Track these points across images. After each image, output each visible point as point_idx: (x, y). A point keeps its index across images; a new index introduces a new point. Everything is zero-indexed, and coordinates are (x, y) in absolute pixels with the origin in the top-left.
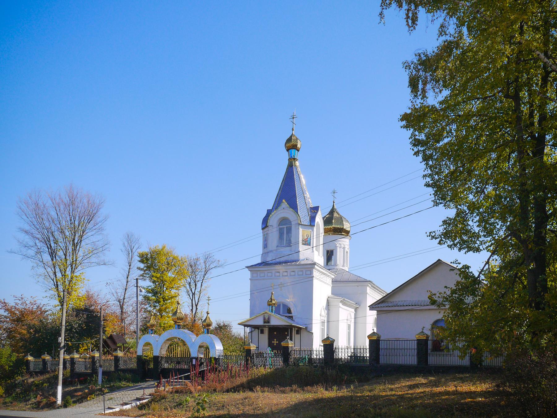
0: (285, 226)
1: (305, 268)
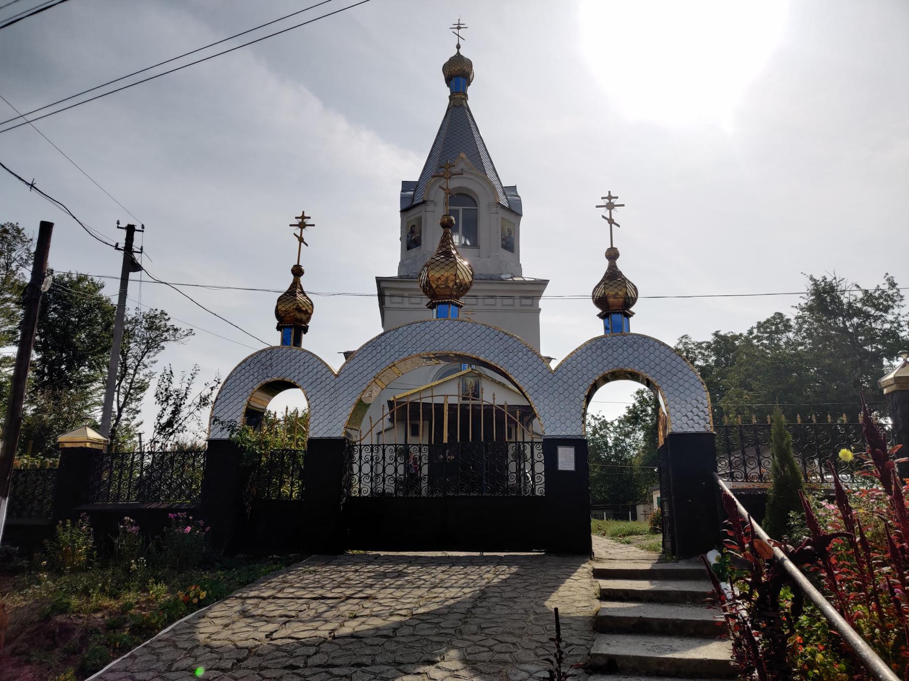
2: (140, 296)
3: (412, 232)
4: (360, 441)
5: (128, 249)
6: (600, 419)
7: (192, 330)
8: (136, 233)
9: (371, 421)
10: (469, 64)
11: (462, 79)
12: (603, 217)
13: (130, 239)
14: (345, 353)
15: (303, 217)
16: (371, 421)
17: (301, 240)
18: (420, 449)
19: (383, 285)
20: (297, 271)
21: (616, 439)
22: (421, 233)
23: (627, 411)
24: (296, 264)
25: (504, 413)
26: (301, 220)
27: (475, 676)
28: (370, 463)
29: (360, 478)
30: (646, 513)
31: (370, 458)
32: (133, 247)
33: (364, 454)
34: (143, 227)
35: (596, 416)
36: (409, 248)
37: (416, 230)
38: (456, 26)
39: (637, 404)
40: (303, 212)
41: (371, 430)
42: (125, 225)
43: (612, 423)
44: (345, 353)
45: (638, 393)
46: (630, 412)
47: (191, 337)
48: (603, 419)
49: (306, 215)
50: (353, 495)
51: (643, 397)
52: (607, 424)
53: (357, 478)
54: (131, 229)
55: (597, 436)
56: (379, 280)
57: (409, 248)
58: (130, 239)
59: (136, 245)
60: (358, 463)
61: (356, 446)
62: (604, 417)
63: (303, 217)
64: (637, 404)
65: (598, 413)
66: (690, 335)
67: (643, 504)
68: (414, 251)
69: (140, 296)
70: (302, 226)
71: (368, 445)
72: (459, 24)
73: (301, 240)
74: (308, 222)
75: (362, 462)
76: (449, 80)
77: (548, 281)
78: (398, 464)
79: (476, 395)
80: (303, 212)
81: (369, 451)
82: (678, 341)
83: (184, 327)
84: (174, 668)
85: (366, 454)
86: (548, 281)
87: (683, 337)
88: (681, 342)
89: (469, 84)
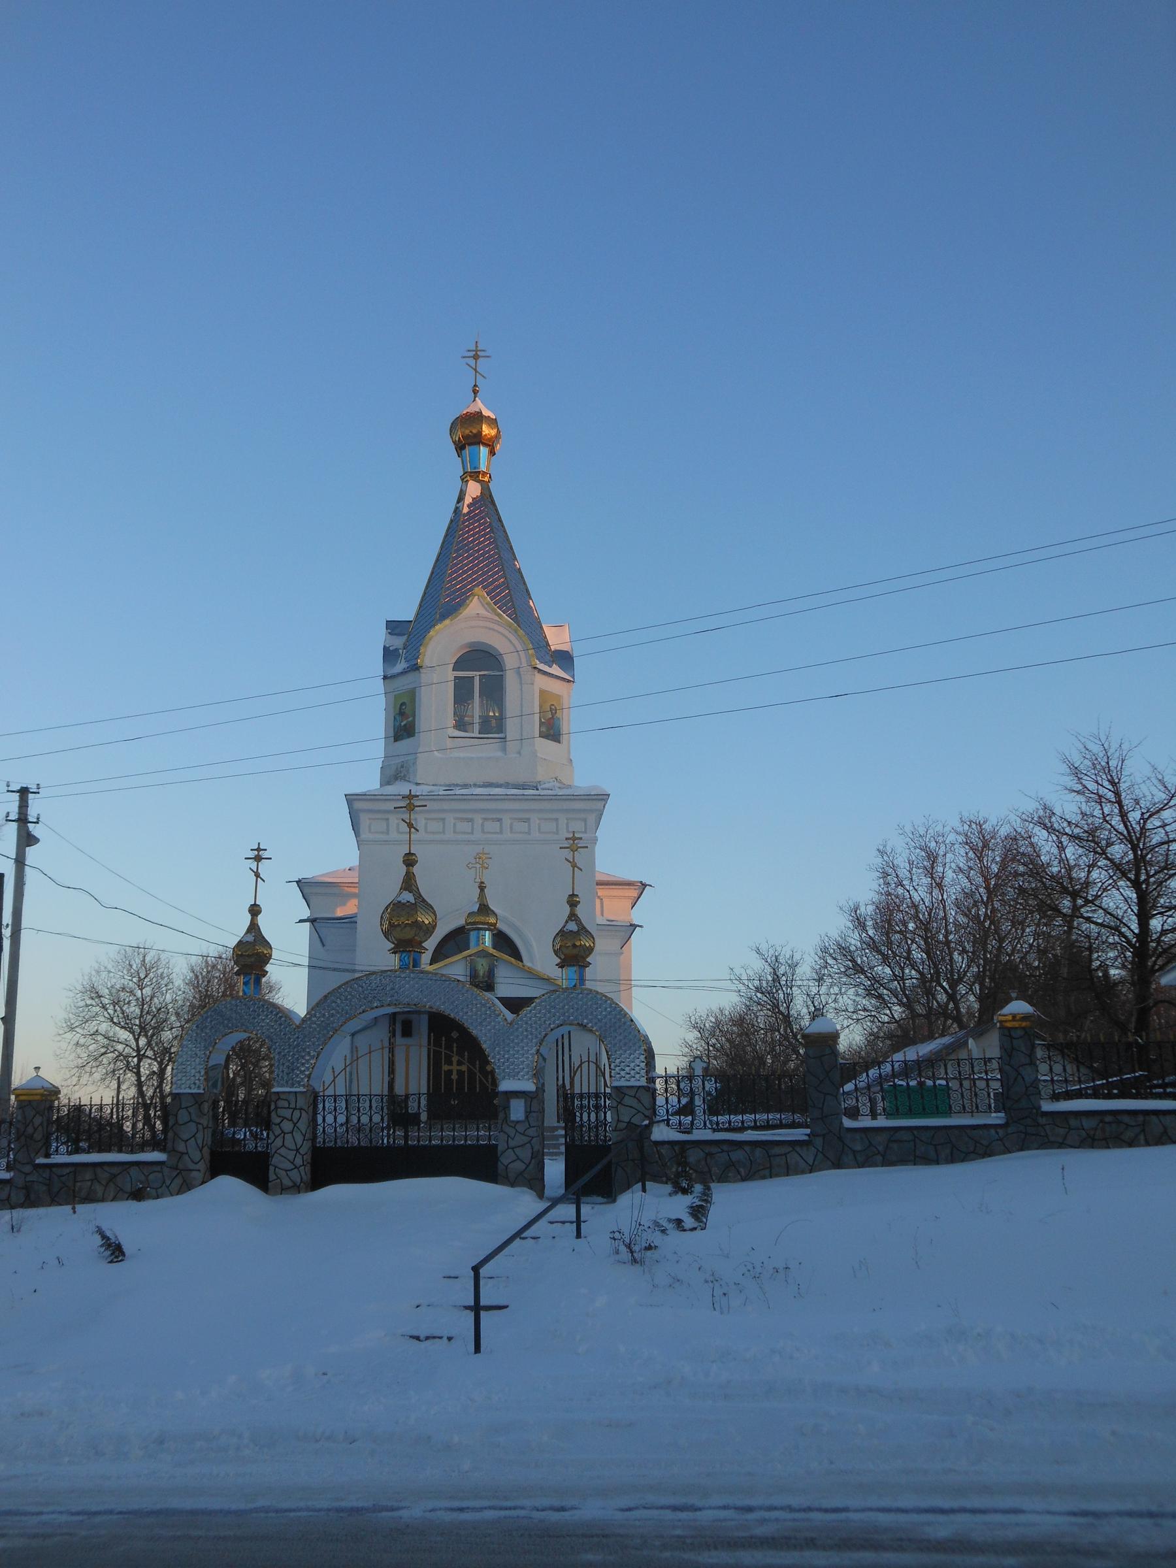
0: (476, 674)
1: (567, 811)
4: (324, 1091)
5: (23, 819)
8: (31, 796)
9: (334, 1072)
12: (566, 859)
13: (23, 805)
14: (298, 882)
15: (259, 849)
16: (334, 1072)
17: (257, 875)
18: (382, 1099)
19: (358, 805)
20: (255, 910)
22: (414, 716)
24: (253, 903)
25: (468, 1062)
26: (256, 852)
27: (136, 1085)
28: (334, 1113)
29: (324, 1128)
31: (333, 1108)
32: (29, 817)
33: (327, 1105)
34: (38, 786)
36: (397, 738)
37: (408, 711)
38: (472, 354)
40: (259, 844)
41: (334, 1080)
42: (18, 788)
44: (298, 882)
49: (262, 847)
50: (318, 1145)
53: (322, 1129)
54: (24, 792)
56: (351, 799)
57: (397, 738)
58: (23, 805)
59: (32, 814)
60: (322, 1113)
61: (320, 1096)
63: (259, 849)
68: (405, 745)
70: (258, 859)
71: (331, 1096)
72: (476, 351)
73: (257, 875)
74: (264, 854)
75: (326, 1113)
78: (361, 1114)
80: (259, 844)
81: (333, 1101)
84: (1080, 787)
85: (329, 1105)
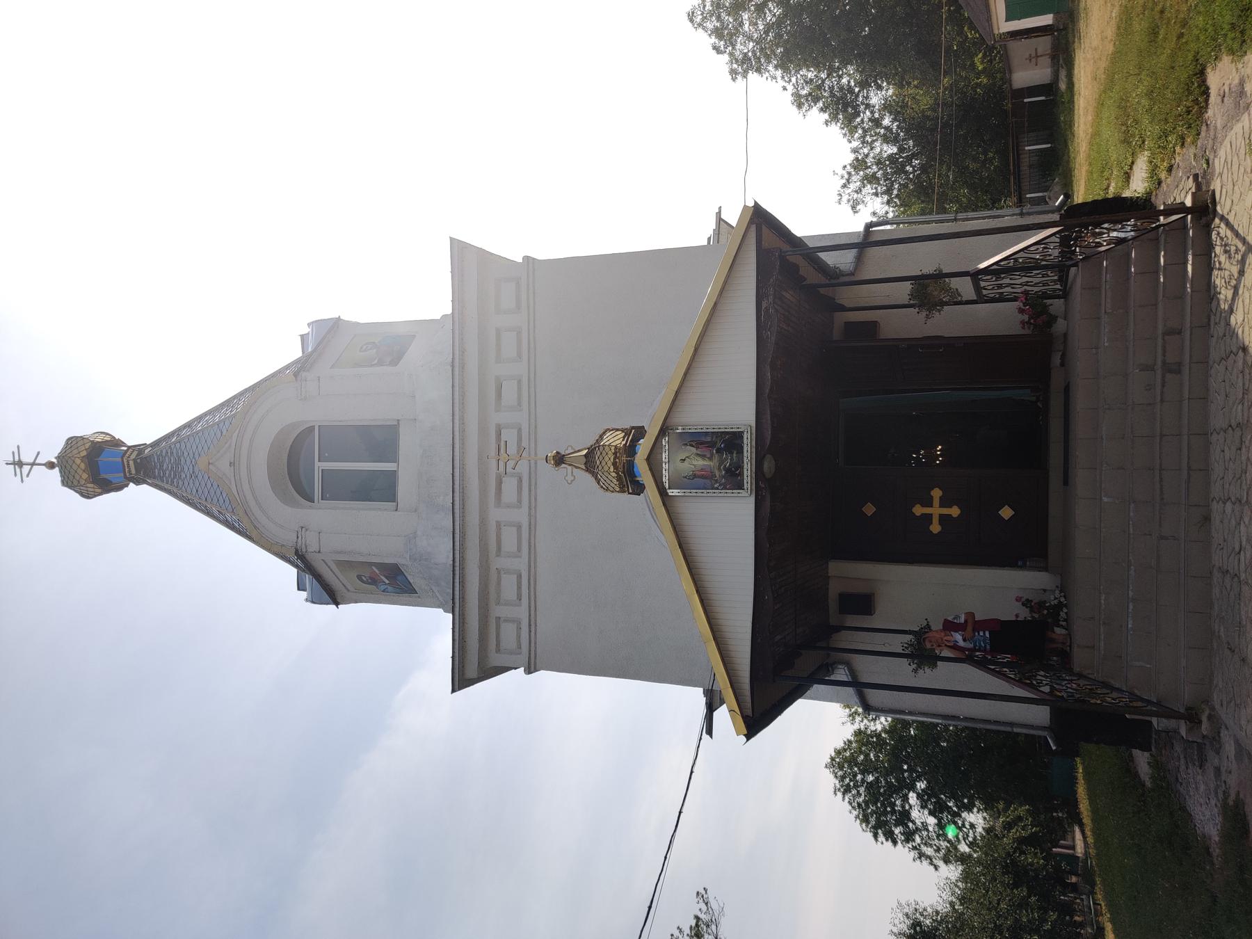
2: (1041, 56)
3: (373, 581)
6: (849, 174)
7: (698, 893)
10: (72, 442)
11: (103, 458)
19: (472, 672)
21: (886, 140)
23: (833, 123)
30: (1033, 55)
35: (844, 181)
39: (820, 104)
43: (855, 151)
45: (800, 106)
46: (834, 118)
47: (711, 896)
48: (848, 167)
51: (807, 96)
52: (857, 159)
55: (879, 174)
62: (845, 167)
64: (820, 104)
65: (838, 178)
66: (689, 9)
67: (1010, 72)
69: (1041, 56)
76: (107, 486)
77: (452, 240)
79: (729, 442)
82: (700, 30)
83: (696, 908)
86: (452, 240)
87: (691, 21)
88: (700, 25)
89: (117, 443)
